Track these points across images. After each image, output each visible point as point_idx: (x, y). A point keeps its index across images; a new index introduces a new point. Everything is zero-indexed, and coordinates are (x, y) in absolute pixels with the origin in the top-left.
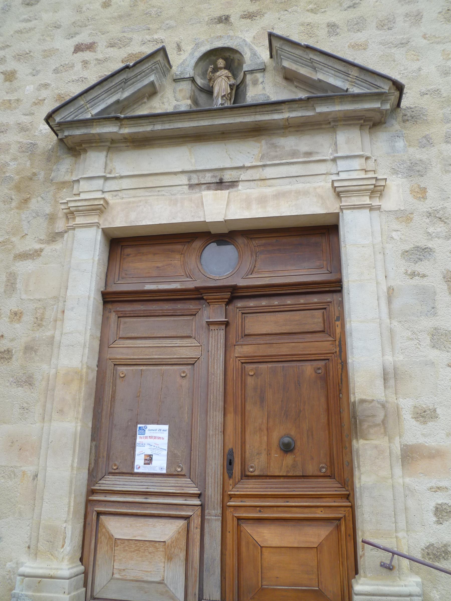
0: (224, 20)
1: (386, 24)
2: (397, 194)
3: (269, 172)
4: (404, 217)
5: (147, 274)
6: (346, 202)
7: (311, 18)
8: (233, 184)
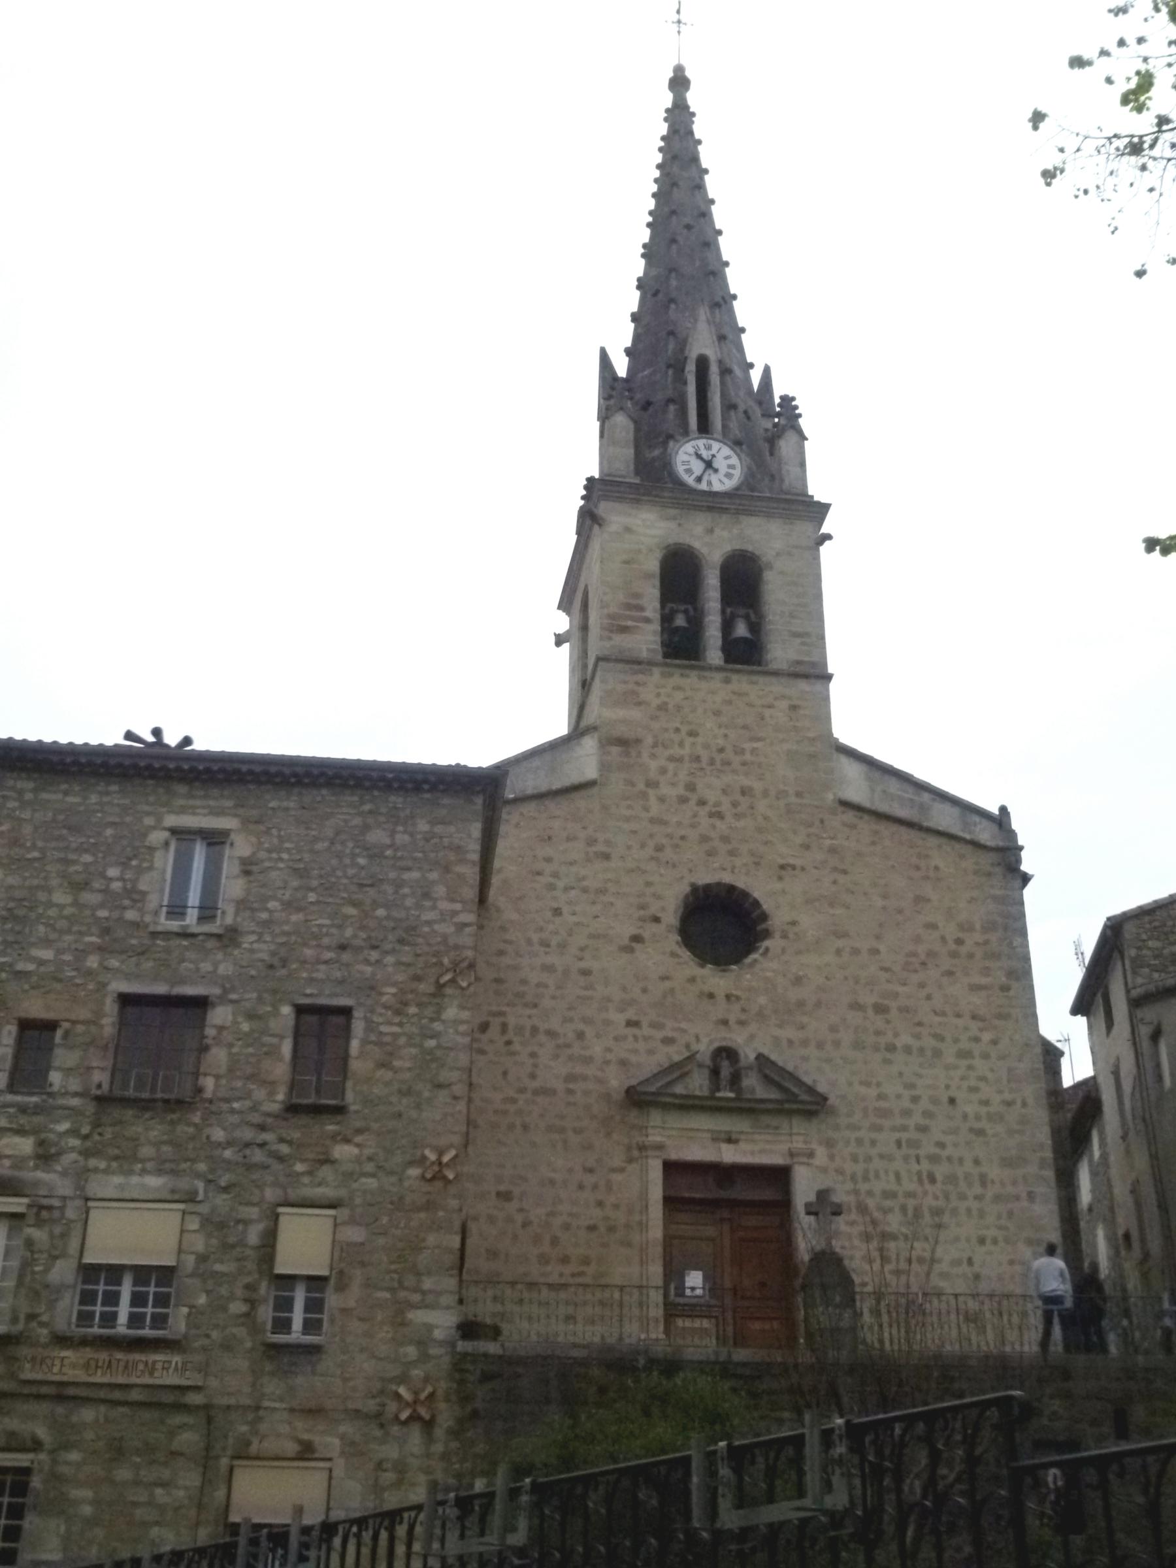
0: (725, 1022)
1: (820, 1045)
2: (821, 1154)
3: (757, 1137)
4: (824, 1170)
5: (696, 1191)
6: (795, 1160)
7: (778, 1032)
8: (736, 1142)
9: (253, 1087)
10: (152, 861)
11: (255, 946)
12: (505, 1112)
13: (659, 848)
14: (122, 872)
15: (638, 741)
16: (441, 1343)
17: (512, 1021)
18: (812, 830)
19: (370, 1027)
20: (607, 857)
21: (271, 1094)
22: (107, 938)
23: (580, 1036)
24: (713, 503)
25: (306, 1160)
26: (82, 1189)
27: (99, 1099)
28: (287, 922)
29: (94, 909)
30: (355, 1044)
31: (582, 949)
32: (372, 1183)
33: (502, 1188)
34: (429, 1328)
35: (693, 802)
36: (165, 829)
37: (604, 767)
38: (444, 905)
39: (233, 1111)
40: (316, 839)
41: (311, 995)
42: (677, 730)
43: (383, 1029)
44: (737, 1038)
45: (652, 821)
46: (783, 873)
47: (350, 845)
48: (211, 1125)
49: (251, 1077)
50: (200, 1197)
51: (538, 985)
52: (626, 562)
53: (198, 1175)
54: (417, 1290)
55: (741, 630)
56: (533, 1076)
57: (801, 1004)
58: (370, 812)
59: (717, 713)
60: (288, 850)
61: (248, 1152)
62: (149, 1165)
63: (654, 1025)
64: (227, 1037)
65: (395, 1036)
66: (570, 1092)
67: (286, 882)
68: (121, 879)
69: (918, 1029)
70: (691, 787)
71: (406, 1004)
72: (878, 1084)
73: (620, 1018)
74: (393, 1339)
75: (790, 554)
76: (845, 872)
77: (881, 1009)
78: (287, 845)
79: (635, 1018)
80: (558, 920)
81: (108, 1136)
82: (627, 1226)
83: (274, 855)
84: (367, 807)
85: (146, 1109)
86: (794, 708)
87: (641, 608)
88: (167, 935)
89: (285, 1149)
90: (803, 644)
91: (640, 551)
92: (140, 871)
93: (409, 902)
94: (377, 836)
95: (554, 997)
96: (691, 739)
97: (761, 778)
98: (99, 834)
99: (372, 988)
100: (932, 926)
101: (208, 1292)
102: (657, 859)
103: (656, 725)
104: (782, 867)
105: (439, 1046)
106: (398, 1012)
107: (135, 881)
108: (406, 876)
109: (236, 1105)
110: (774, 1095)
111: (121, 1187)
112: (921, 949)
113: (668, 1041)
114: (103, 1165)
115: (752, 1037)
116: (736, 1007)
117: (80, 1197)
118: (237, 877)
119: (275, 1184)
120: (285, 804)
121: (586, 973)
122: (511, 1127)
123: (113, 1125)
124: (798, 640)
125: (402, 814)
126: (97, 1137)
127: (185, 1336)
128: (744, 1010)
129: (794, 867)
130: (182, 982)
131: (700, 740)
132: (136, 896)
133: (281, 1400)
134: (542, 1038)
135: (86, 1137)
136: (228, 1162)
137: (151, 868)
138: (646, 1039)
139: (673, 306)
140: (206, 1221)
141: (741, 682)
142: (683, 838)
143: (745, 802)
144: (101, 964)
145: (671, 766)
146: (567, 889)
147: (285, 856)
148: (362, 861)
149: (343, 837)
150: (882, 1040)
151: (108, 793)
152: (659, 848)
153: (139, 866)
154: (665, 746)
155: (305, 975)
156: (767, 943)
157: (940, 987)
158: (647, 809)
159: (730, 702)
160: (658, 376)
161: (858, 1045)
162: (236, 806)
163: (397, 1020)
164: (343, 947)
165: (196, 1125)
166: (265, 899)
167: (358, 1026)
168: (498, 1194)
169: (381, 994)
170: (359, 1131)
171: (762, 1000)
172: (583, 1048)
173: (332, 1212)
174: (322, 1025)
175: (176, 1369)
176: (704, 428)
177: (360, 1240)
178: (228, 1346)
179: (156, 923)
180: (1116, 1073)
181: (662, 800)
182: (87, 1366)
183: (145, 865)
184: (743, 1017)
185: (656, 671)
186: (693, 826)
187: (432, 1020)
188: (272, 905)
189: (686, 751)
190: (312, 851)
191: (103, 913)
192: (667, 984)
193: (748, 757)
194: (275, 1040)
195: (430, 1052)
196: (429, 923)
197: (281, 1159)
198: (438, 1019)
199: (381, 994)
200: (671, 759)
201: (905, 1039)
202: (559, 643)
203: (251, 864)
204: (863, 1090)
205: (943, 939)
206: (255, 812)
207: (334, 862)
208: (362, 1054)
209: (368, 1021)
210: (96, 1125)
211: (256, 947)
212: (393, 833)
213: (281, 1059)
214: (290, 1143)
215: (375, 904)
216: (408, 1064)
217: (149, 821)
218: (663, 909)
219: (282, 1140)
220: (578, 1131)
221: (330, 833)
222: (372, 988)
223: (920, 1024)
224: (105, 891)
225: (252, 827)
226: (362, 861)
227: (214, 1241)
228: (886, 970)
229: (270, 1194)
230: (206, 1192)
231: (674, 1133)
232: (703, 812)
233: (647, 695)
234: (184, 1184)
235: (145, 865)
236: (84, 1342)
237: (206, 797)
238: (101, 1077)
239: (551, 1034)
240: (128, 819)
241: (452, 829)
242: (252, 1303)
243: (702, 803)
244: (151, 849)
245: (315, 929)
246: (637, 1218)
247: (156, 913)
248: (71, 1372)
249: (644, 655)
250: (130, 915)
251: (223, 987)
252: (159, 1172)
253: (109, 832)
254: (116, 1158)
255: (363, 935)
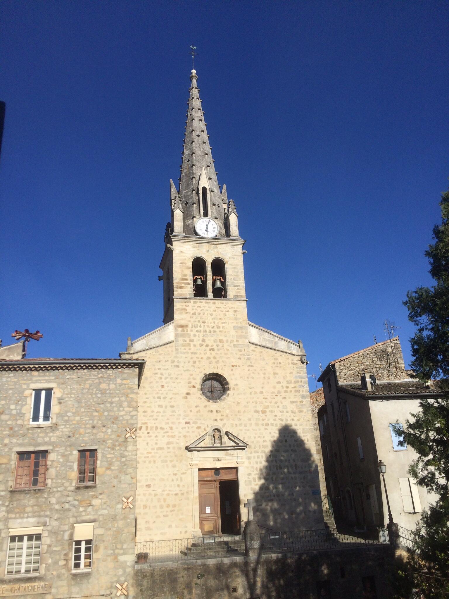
0: (216, 420)
8: (221, 460)
9: (64, 481)
10: (26, 402)
11: (64, 430)
12: (148, 457)
13: (194, 362)
14: (16, 407)
15: (187, 326)
16: (130, 567)
17: (149, 425)
18: (241, 353)
19: (104, 456)
20: (178, 366)
21: (71, 484)
22: (11, 432)
23: (171, 428)
24: (209, 241)
25: (83, 507)
26: (7, 525)
27: (11, 492)
28: (74, 420)
29: (7, 421)
30: (98, 462)
31: (171, 399)
32: (105, 512)
33: (147, 484)
34: (126, 562)
35: (204, 346)
36: (30, 389)
37: (176, 336)
38: (127, 409)
39: (58, 491)
40: (83, 389)
41: (83, 446)
42: (199, 321)
43: (108, 456)
44: (219, 425)
45: (192, 353)
46: (233, 368)
47: (95, 390)
48: (50, 497)
49: (64, 478)
50: (48, 524)
51: (157, 412)
52: (181, 263)
53: (47, 516)
54: (122, 549)
55: (218, 284)
56: (156, 444)
57: (239, 412)
58: (101, 377)
59: (211, 315)
60: (74, 394)
61: (63, 505)
62: (30, 514)
63: (194, 423)
64: (55, 464)
65: (112, 458)
66: (169, 448)
67: (73, 405)
68: (16, 409)
69: (275, 417)
70: (203, 341)
71: (115, 445)
72: (264, 437)
73: (183, 422)
74: (115, 567)
75: (233, 258)
76: (252, 366)
77: (264, 412)
78: (74, 392)
79: (188, 421)
80: (163, 389)
81: (15, 505)
82: (187, 492)
83: (69, 396)
84: (100, 376)
85: (27, 493)
86: (235, 311)
87: (186, 279)
88: (33, 428)
89: (76, 503)
90: (238, 289)
91: (185, 259)
92: (22, 406)
93: (115, 409)
94: (104, 386)
95: (162, 416)
96: (204, 324)
97: (226, 336)
98: (7, 392)
99: (104, 441)
100: (279, 383)
101: (52, 558)
102: (194, 366)
103: (192, 320)
104: (233, 366)
105: (126, 460)
106: (113, 449)
107: (20, 410)
108: (114, 400)
109: (59, 489)
110: (233, 444)
111: (20, 523)
112: (276, 391)
113: (198, 428)
114: (13, 516)
115: (224, 424)
116: (219, 414)
117: (6, 528)
118: (56, 405)
119: (74, 516)
120: (72, 377)
121: (172, 407)
122: (150, 462)
123: (16, 501)
124: (236, 288)
125: (112, 377)
126: (11, 506)
127: (45, 575)
128: (222, 415)
129: (236, 366)
130: (39, 445)
131: (206, 324)
132: (21, 415)
133: (78, 593)
134: (159, 430)
135: (8, 506)
136: (57, 510)
137: (26, 404)
138: (192, 427)
139: (194, 167)
140: (50, 532)
141: (219, 302)
142: (201, 358)
143: (221, 344)
144: (10, 441)
145: (197, 334)
146: (166, 378)
147: (73, 396)
148: (99, 395)
149: (92, 387)
150: (264, 422)
151: (9, 377)
152: (194, 362)
153: (22, 404)
154: (195, 327)
155: (81, 439)
156: (229, 392)
157: (282, 403)
158: (190, 349)
159: (215, 311)
160: (190, 193)
161: (257, 424)
162: (55, 379)
163: (112, 452)
164: (94, 427)
165: (45, 498)
166: (67, 412)
167: (99, 455)
168: (146, 486)
169: (107, 443)
170: (101, 494)
171: (227, 411)
172: (172, 433)
173: (93, 524)
174: (88, 455)
175: (42, 587)
176: (206, 214)
177: (102, 533)
178: (59, 576)
179: (29, 424)
180: (332, 404)
181: (195, 346)
182: (11, 590)
183: (24, 403)
184: (222, 418)
185: (192, 301)
186: (205, 354)
187: (124, 451)
188: (69, 414)
189: (202, 329)
190: (82, 393)
191: (9, 423)
192: (198, 408)
193: (221, 329)
194: (72, 464)
195: (124, 462)
196: (122, 416)
197: (74, 506)
198: (126, 450)
199: (107, 443)
200: (197, 331)
201: (271, 421)
202: (160, 280)
203: (62, 399)
204: (259, 439)
205: (282, 386)
206: (61, 380)
207: (90, 396)
208: (101, 467)
209: (103, 453)
210: (11, 501)
211: (64, 430)
212: (109, 384)
213: (73, 470)
214: (78, 500)
215: (104, 411)
216: (117, 468)
217: (25, 387)
218: (196, 383)
219: (75, 500)
220: (171, 461)
221: (88, 386)
222: (104, 441)
223: (276, 416)
224: (10, 414)
225: (61, 386)
226: (99, 395)
227: (53, 539)
228: (266, 398)
229: (72, 520)
230: (49, 521)
231: (201, 459)
232: (208, 348)
233: (189, 309)
234: (42, 520)
235: (24, 403)
236: (10, 581)
237: (44, 376)
238: (11, 483)
239: (162, 428)
240: (17, 386)
241: (129, 381)
242: (67, 560)
243: (207, 346)
244: (26, 397)
245: (84, 422)
246: (190, 489)
247: (29, 420)
248: (6, 593)
249: (188, 296)
250: (20, 422)
251: (53, 446)
252: (33, 517)
253: (10, 392)
254: (18, 513)
255: (100, 422)
